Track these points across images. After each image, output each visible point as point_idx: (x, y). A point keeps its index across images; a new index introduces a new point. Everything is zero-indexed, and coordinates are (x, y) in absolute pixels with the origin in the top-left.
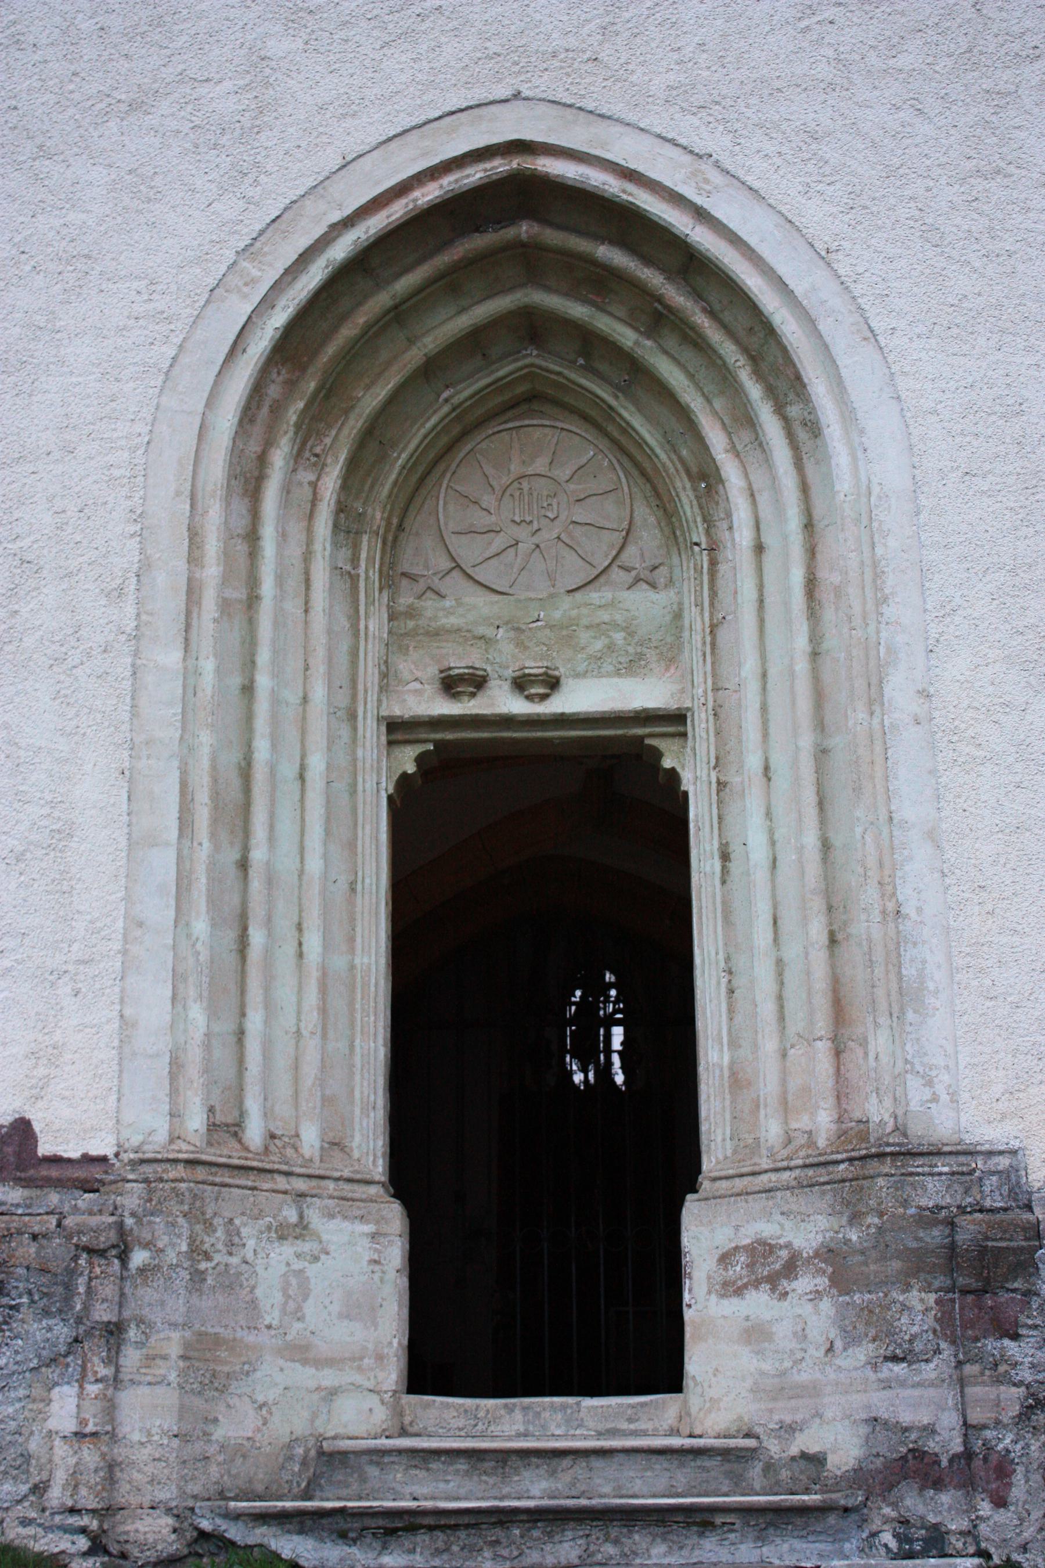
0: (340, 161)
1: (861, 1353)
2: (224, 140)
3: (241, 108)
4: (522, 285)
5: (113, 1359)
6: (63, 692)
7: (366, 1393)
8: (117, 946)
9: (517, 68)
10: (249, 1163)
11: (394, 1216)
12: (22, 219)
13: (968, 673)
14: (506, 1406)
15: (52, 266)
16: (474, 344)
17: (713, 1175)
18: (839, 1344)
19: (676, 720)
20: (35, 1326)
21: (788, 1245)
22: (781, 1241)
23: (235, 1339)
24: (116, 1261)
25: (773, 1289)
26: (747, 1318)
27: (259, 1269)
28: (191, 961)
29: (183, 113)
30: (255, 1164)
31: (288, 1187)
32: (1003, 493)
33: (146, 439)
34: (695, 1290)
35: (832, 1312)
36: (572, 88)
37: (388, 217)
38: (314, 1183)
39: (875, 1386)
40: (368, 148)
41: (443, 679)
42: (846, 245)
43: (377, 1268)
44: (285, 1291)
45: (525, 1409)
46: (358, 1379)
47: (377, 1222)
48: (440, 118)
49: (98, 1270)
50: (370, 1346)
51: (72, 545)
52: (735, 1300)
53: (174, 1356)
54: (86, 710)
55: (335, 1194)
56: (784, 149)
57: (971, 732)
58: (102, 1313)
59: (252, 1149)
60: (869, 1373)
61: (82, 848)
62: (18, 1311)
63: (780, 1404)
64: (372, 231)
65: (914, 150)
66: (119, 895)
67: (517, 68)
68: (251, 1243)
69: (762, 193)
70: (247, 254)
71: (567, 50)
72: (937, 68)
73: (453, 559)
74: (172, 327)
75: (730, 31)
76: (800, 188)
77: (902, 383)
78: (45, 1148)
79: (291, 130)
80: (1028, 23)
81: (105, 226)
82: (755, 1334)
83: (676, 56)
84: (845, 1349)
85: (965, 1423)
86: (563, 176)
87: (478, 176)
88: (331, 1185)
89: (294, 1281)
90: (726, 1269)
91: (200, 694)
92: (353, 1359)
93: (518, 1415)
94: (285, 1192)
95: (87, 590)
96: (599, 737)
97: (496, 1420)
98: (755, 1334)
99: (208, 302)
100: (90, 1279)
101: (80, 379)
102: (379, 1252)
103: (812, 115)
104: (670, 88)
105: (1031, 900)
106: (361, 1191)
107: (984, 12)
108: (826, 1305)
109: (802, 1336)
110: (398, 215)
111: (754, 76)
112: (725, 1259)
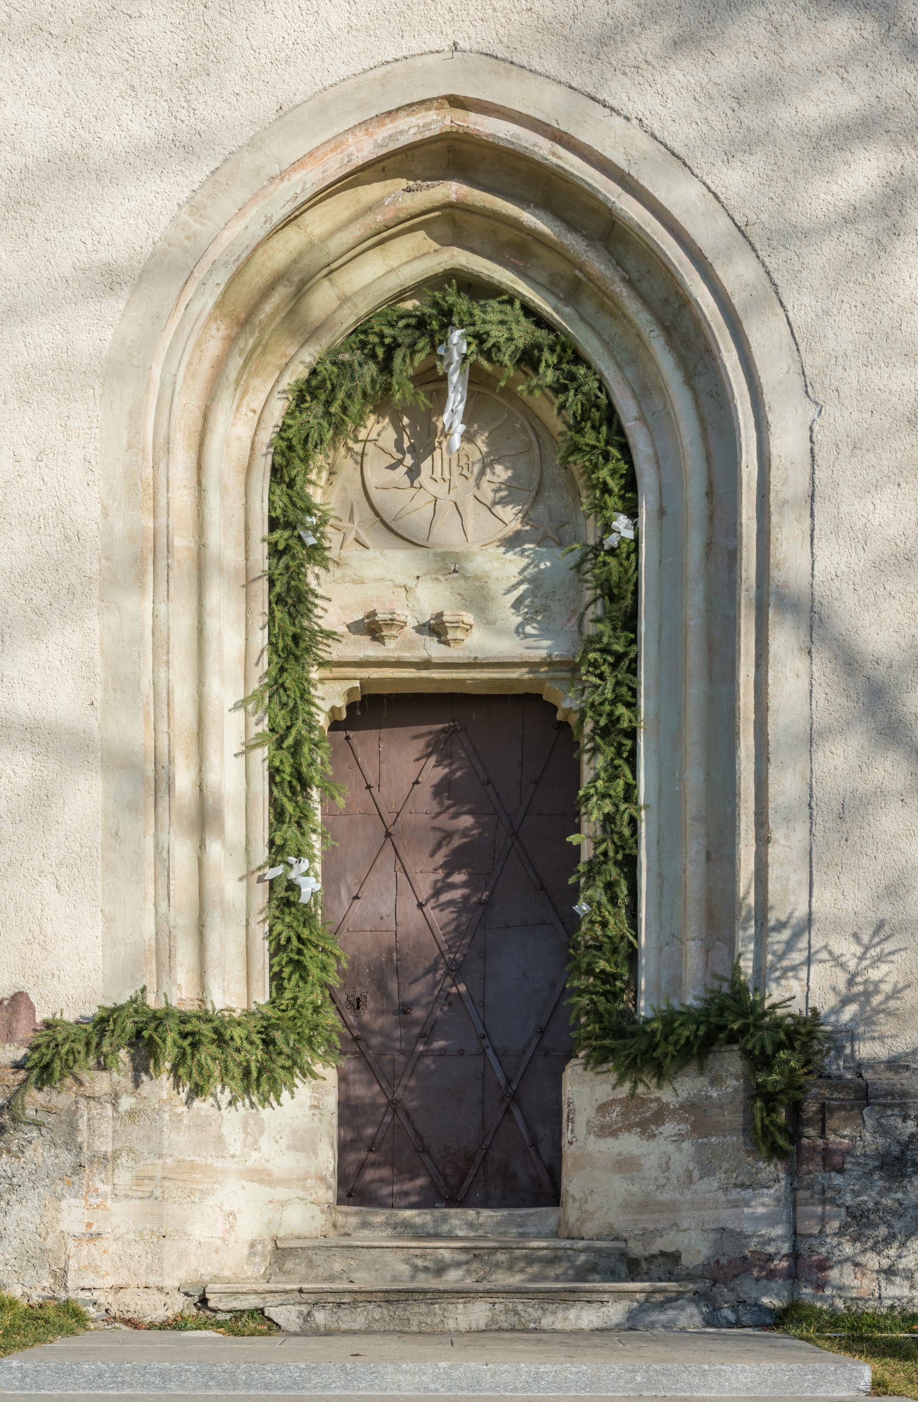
18: (696, 1174)
23: (206, 1165)
25: (643, 1133)
26: (620, 1154)
34: (577, 1131)
35: (692, 1150)
39: (725, 1205)
43: (316, 1112)
49: (94, 1112)
50: (312, 1171)
60: (720, 1194)
84: (701, 1178)
85: (795, 1233)
90: (603, 1116)
92: (299, 1180)
98: (626, 1165)
102: (319, 1100)
109: (666, 1167)
112: (603, 1109)
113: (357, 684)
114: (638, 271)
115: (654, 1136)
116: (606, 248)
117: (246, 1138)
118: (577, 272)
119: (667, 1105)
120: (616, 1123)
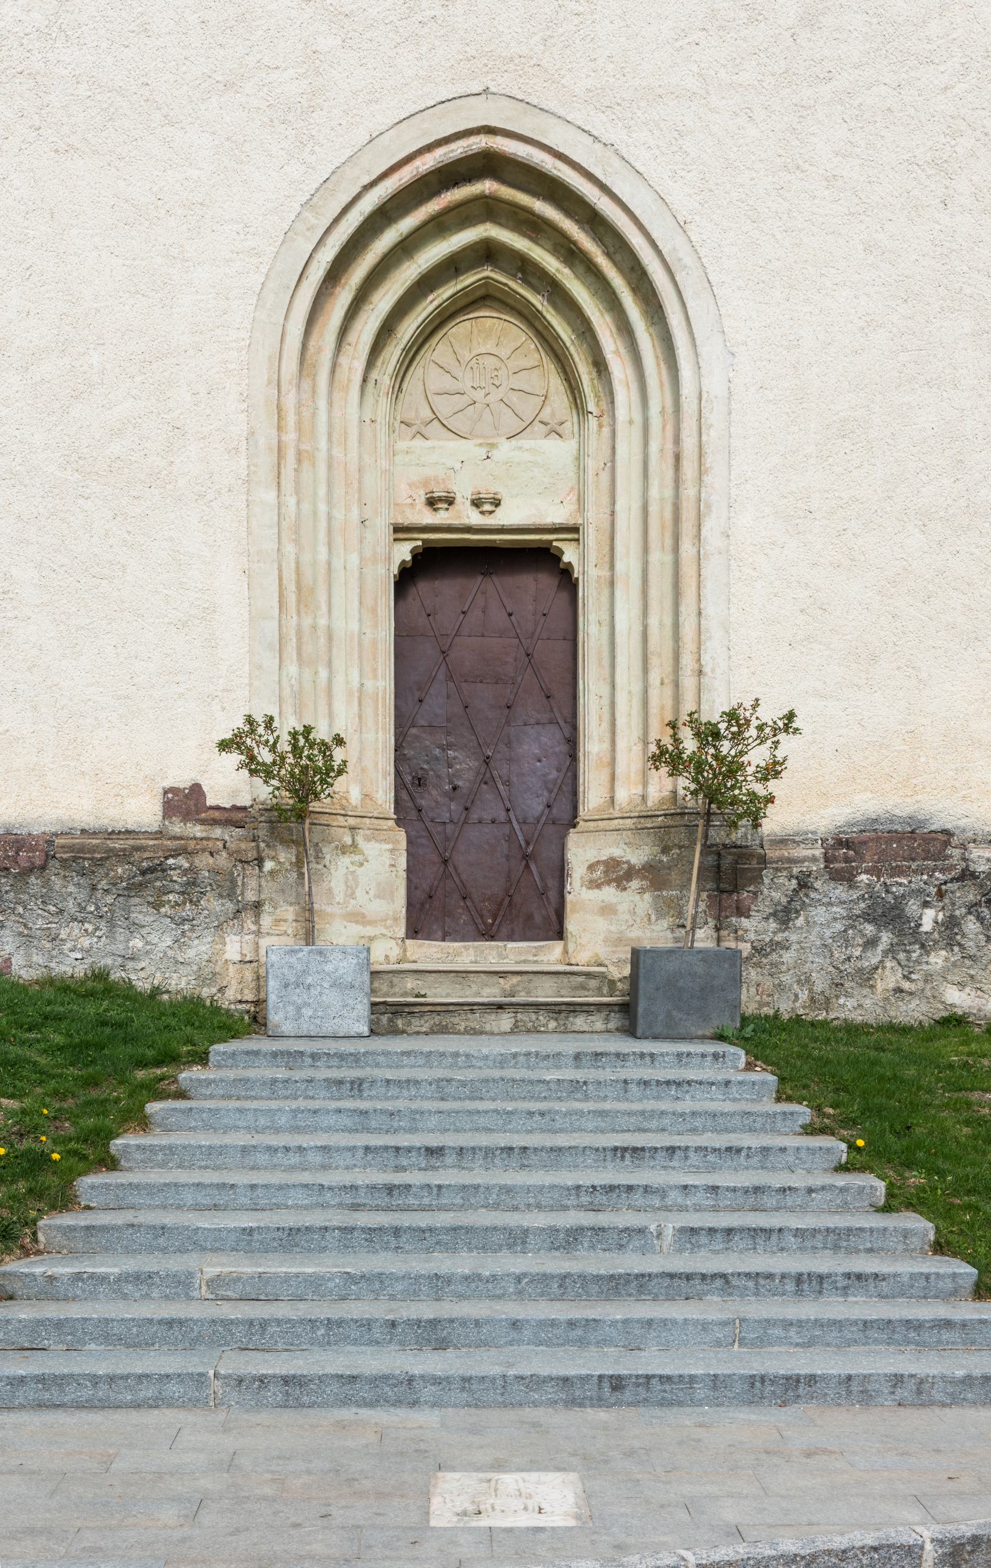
0: (368, 138)
1: (665, 923)
3: (300, 91)
4: (483, 221)
8: (246, 681)
9: (485, 69)
11: (401, 836)
12: (156, 173)
14: (465, 947)
16: (452, 266)
17: (586, 818)
18: (653, 918)
21: (628, 862)
22: (624, 859)
25: (618, 886)
26: (603, 901)
27: (332, 871)
28: (289, 689)
29: (261, 94)
30: (327, 810)
33: (248, 343)
34: (574, 884)
35: (650, 900)
37: (400, 180)
41: (428, 499)
42: (697, 218)
43: (393, 869)
44: (346, 883)
45: (474, 947)
46: (384, 931)
47: (393, 843)
50: (391, 913)
52: (596, 891)
57: (750, 560)
58: (251, 896)
60: (668, 933)
63: (619, 949)
67: (485, 69)
68: (328, 857)
72: (764, 84)
74: (261, 260)
78: (210, 802)
82: (607, 910)
86: (515, 154)
87: (459, 151)
88: (367, 821)
89: (350, 877)
90: (592, 873)
91: (287, 519)
92: (382, 920)
93: (471, 951)
94: (345, 827)
95: (216, 449)
97: (458, 954)
99: (283, 242)
101: (203, 297)
102: (395, 860)
108: (647, 896)
110: (406, 179)
112: (591, 868)
113: (420, 543)
115: (626, 889)
116: (592, 229)
119: (634, 866)
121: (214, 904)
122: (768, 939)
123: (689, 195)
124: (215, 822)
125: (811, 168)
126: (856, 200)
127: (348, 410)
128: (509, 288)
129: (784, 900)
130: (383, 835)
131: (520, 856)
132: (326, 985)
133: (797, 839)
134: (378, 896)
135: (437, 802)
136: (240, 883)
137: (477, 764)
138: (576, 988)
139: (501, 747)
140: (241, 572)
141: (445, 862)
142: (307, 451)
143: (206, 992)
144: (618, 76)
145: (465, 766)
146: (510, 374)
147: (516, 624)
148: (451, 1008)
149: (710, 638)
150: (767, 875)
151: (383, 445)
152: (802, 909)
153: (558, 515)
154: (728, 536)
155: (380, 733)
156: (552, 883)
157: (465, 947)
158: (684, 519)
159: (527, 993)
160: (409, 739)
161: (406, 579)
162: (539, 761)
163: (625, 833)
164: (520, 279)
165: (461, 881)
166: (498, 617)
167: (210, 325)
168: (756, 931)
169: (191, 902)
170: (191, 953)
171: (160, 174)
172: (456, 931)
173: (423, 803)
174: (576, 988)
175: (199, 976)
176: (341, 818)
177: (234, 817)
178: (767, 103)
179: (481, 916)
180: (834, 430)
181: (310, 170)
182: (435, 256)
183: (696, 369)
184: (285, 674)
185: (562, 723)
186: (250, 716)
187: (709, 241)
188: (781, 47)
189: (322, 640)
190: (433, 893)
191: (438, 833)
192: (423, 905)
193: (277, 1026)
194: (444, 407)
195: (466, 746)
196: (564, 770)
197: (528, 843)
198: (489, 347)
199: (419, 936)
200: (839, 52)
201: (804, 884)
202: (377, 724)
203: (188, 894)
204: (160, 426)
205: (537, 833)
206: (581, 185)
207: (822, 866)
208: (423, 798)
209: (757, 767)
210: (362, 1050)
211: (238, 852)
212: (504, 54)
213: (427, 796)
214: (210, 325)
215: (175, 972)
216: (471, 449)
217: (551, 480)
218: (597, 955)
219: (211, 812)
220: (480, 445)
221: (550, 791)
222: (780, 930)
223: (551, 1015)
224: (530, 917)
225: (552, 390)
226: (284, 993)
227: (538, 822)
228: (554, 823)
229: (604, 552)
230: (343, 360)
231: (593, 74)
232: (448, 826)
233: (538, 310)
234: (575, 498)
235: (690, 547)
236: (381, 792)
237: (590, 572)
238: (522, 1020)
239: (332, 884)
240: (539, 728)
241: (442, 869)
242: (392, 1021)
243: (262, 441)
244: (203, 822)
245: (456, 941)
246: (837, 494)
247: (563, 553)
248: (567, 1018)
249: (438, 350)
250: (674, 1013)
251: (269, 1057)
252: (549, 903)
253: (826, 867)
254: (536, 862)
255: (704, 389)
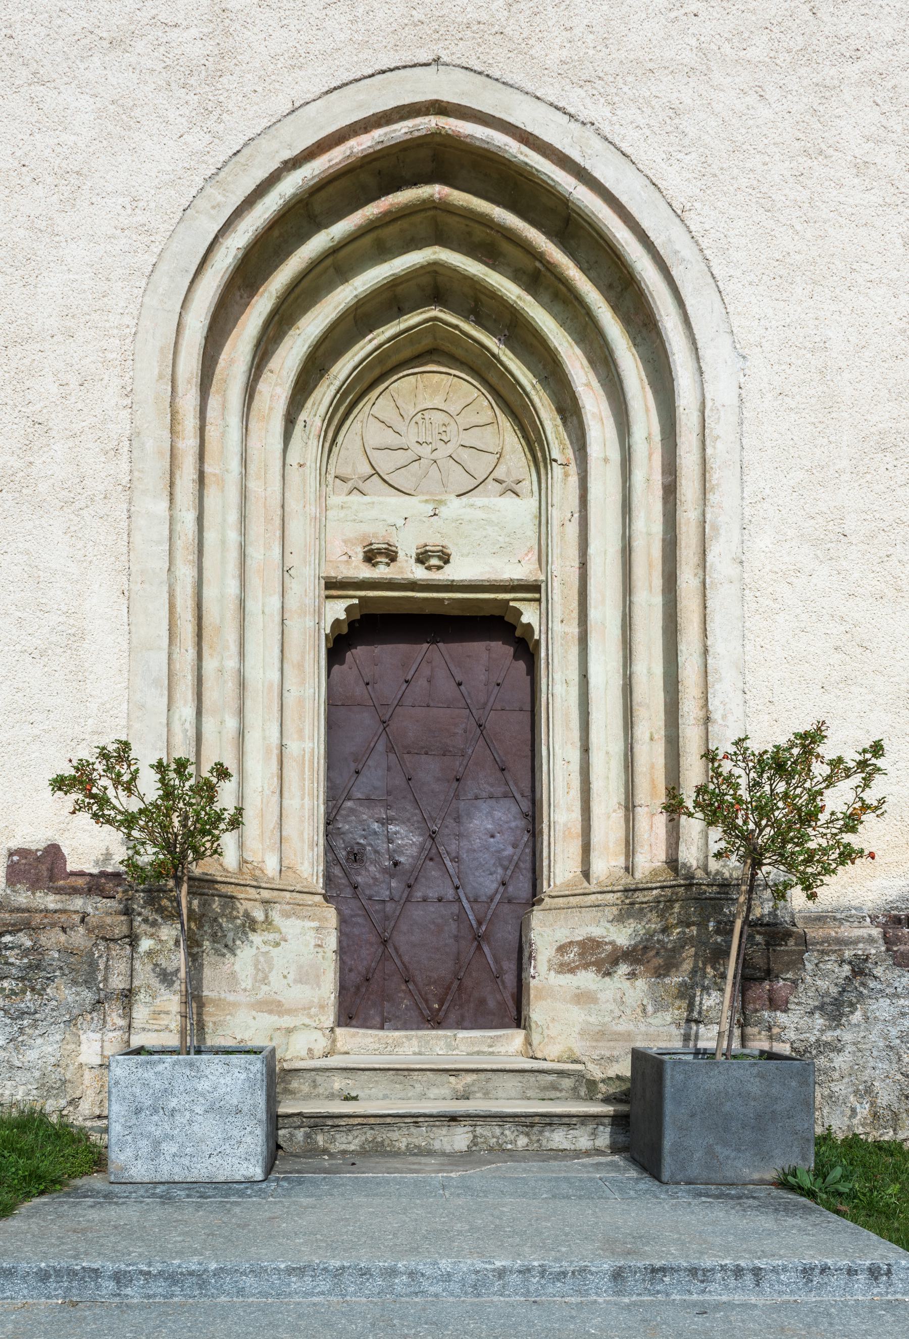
0: (289, 107)
2: (192, 81)
5: (127, 1013)
6: (72, 529)
7: (313, 1030)
8: (124, 722)
10: (228, 880)
11: (331, 914)
12: (20, 136)
13: (770, 546)
14: (407, 1037)
15: (50, 180)
18: (650, 1009)
19: (532, 589)
20: (67, 992)
21: (612, 943)
22: (607, 940)
23: (220, 999)
24: (128, 947)
25: (598, 971)
26: (578, 988)
29: (156, 54)
30: (232, 880)
31: (258, 896)
32: (807, 411)
34: (539, 967)
36: (481, 56)
37: (330, 161)
38: (276, 893)
40: (312, 97)
42: (697, 205)
43: (320, 950)
44: (256, 966)
46: (307, 1021)
47: (320, 920)
48: (373, 75)
50: (316, 1000)
51: (75, 412)
53: (174, 1013)
54: (91, 543)
55: (291, 901)
56: (652, 123)
57: (770, 590)
58: (117, 982)
59: (230, 870)
61: (93, 648)
62: (53, 981)
63: (600, 1044)
64: (316, 172)
65: (755, 131)
66: (123, 685)
67: (436, 36)
69: (633, 158)
70: (214, 181)
71: (479, 23)
72: (778, 62)
73: (375, 469)
75: (613, 17)
76: (664, 156)
77: (735, 321)
79: (249, 76)
80: (852, 29)
81: (93, 148)
82: (583, 998)
83: (568, 34)
87: (403, 131)
88: (288, 895)
89: (262, 959)
90: (562, 955)
91: (183, 538)
92: (305, 1009)
93: (415, 1042)
94: (255, 900)
95: (88, 449)
96: (477, 599)
100: (108, 960)
103: (676, 95)
104: (563, 62)
105: (806, 712)
106: (309, 899)
107: (819, 15)
111: (631, 57)
112: (562, 949)
113: (356, 601)
114: (588, 262)
117: (257, 974)
118: (538, 264)
120: (574, 962)
121: (64, 993)
122: (813, 1039)
123: (688, 180)
124: (74, 891)
125: (836, 153)
126: (893, 190)
127: (253, 436)
128: (461, 331)
129: (834, 991)
130: (306, 912)
131: (471, 937)
132: (199, 1109)
133: (838, 916)
134: (299, 981)
135: (375, 879)
136: (102, 967)
137: (421, 839)
138: (545, 1089)
139: (450, 821)
140: (119, 593)
141: (385, 942)
142: (215, 475)
143: (51, 1105)
144: (598, 48)
145: (407, 840)
146: (461, 429)
147: (466, 694)
148: (388, 1120)
149: (720, 680)
150: (810, 959)
151: (313, 490)
152: (858, 1002)
153: (520, 570)
154: (741, 562)
155: (307, 799)
156: (509, 966)
157: (407, 1037)
158: (683, 545)
159: (485, 1094)
160: (343, 812)
161: (340, 644)
162: (493, 836)
163: (607, 909)
164: (472, 321)
165: (403, 963)
166: (446, 687)
167: (86, 308)
168: (797, 1029)
169: (33, 990)
170: (32, 1055)
171: (25, 137)
172: (397, 1017)
173: (359, 879)
174: (545, 1089)
175: (43, 1085)
176: (252, 890)
177: (98, 884)
178: (783, 82)
179: (426, 1001)
180: (872, 443)
181: (216, 140)
182: (374, 279)
183: (697, 374)
184: (177, 717)
185: (518, 797)
186: (104, 748)
187: (712, 231)
188: (798, 21)
189: (230, 684)
190: (370, 975)
191: (376, 911)
192: (358, 988)
193: (124, 1169)
194: (385, 462)
195: (408, 820)
196: (521, 846)
197: (480, 923)
198: (437, 402)
199: (354, 1022)
200: (869, 29)
201: (860, 969)
202: (303, 789)
203: (30, 980)
204: (16, 421)
205: (490, 912)
206: (553, 172)
207: (883, 949)
208: (360, 874)
209: (833, 814)
210: (213, 1266)
211: (101, 927)
212: (459, 20)
213: (363, 872)
214: (86, 308)
215: (10, 1079)
216: (416, 506)
217: (507, 539)
218: (571, 1050)
219: (73, 879)
220: (427, 501)
221: (506, 869)
222: (830, 1028)
223: (521, 1129)
224: (482, 1002)
225: (507, 448)
226: (134, 1121)
227: (492, 900)
228: (509, 902)
229: (571, 608)
230: (263, 387)
231: (568, 45)
232: (388, 904)
233: (493, 355)
234: (536, 557)
235: (691, 577)
236: (306, 864)
237: (555, 628)
238: (482, 1136)
239: (237, 967)
240: (492, 802)
241: (380, 950)
242: (310, 1137)
243: (150, 445)
244: (59, 891)
245: (397, 1029)
246: (877, 516)
247: (521, 614)
248: (541, 1132)
249: (380, 405)
250: (718, 1149)
251: (31, 1280)
252: (505, 988)
253: (888, 950)
254: (489, 943)
255: (708, 396)
